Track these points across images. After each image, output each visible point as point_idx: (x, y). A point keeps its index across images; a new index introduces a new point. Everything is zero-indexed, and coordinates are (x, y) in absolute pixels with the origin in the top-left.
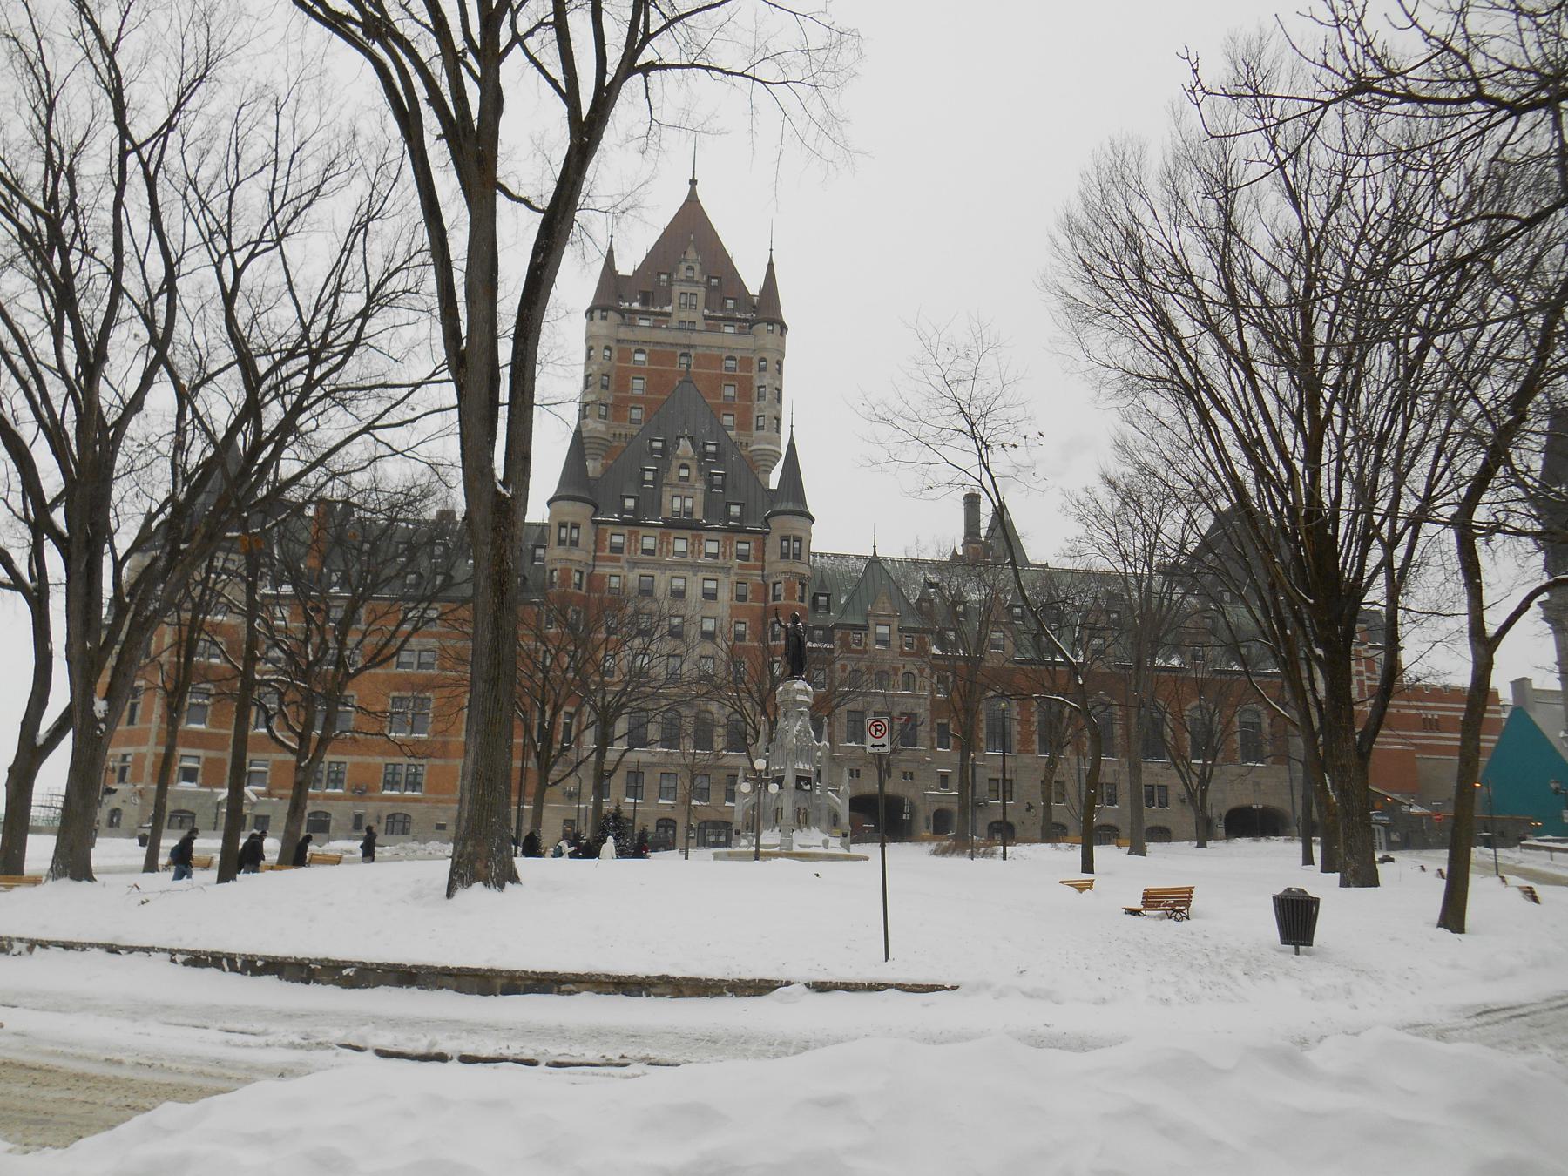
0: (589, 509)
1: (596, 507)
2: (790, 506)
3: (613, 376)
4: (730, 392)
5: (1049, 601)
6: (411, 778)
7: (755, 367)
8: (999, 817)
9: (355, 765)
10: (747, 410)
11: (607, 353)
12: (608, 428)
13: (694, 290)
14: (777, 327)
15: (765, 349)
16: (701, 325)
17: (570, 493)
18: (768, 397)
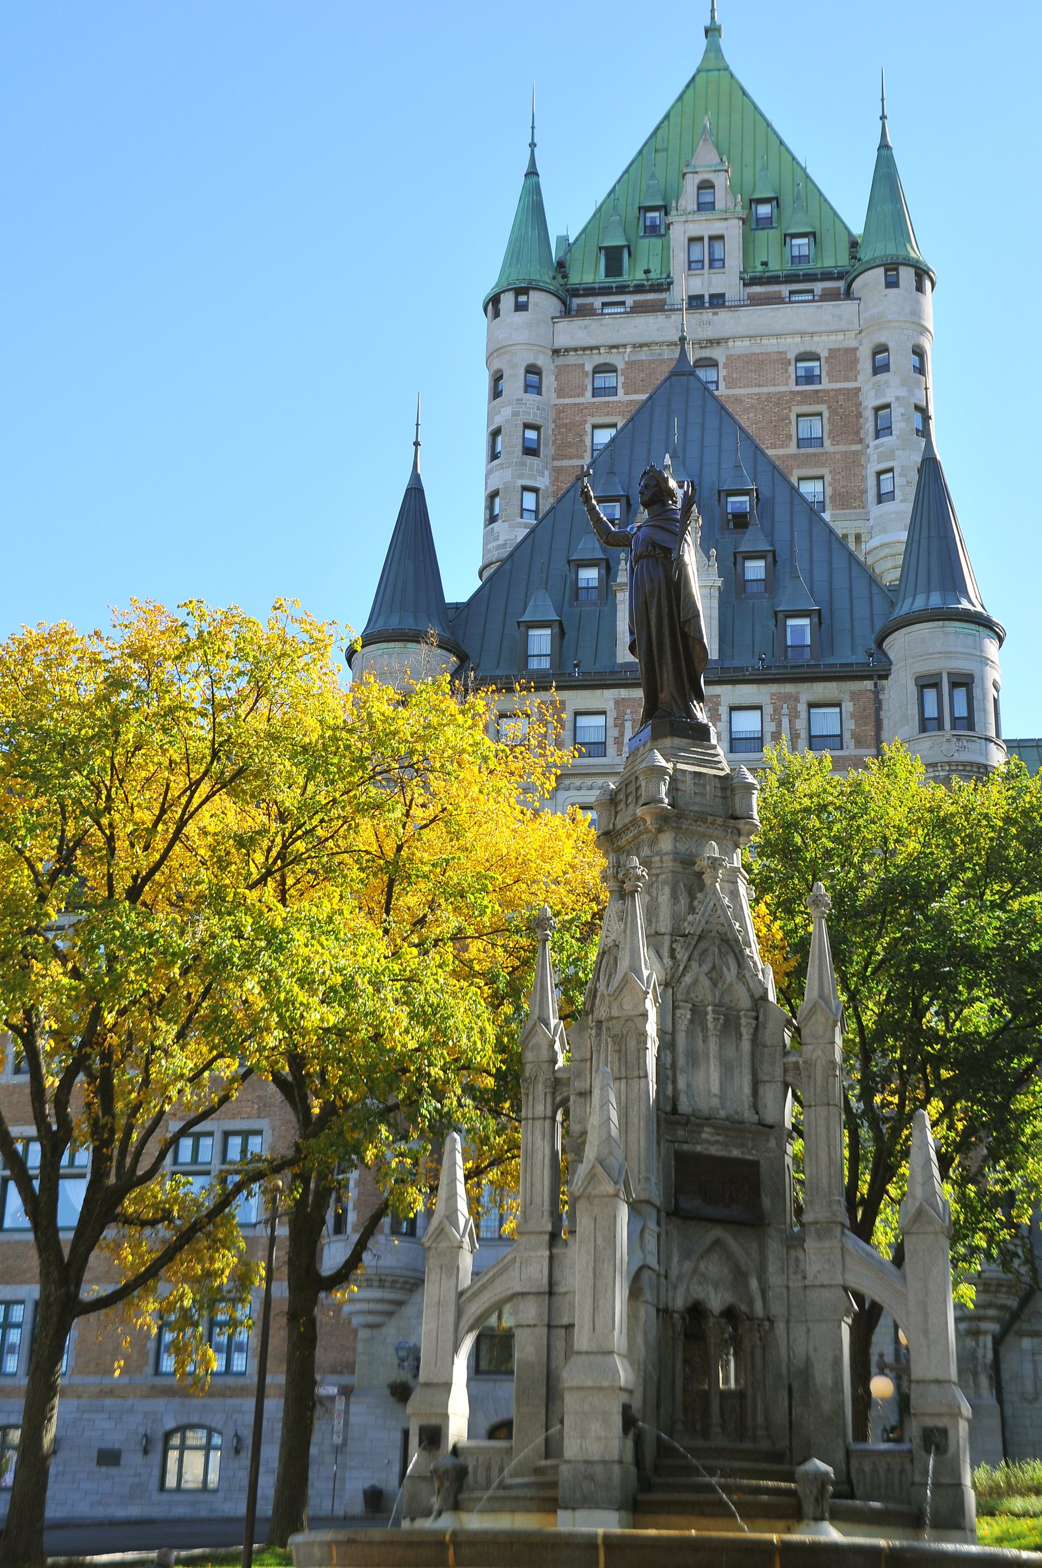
2: (936, 600)
7: (865, 365)
10: (854, 462)
13: (717, 228)
14: (907, 275)
17: (394, 623)
18: (897, 426)
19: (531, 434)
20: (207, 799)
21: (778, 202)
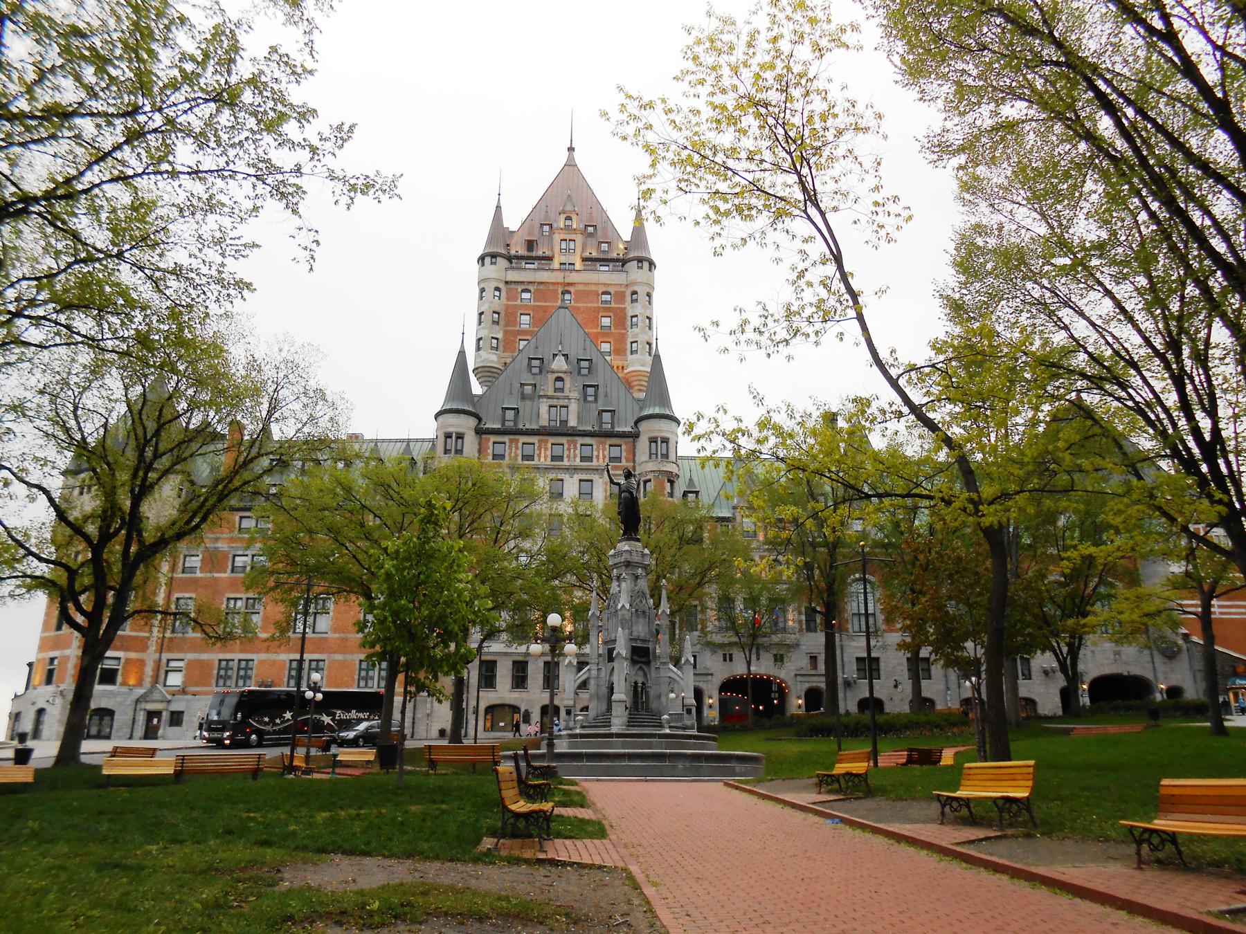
0: (472, 422)
1: (480, 419)
2: (657, 410)
3: (502, 314)
4: (606, 321)
5: (907, 462)
6: (222, 673)
7: (628, 298)
8: (867, 695)
9: (262, 662)
10: (623, 337)
11: (497, 293)
12: (500, 357)
14: (646, 265)
15: (635, 283)
16: (578, 266)
17: (454, 407)
19: (496, 316)
20: (793, 806)
21: (596, 228)
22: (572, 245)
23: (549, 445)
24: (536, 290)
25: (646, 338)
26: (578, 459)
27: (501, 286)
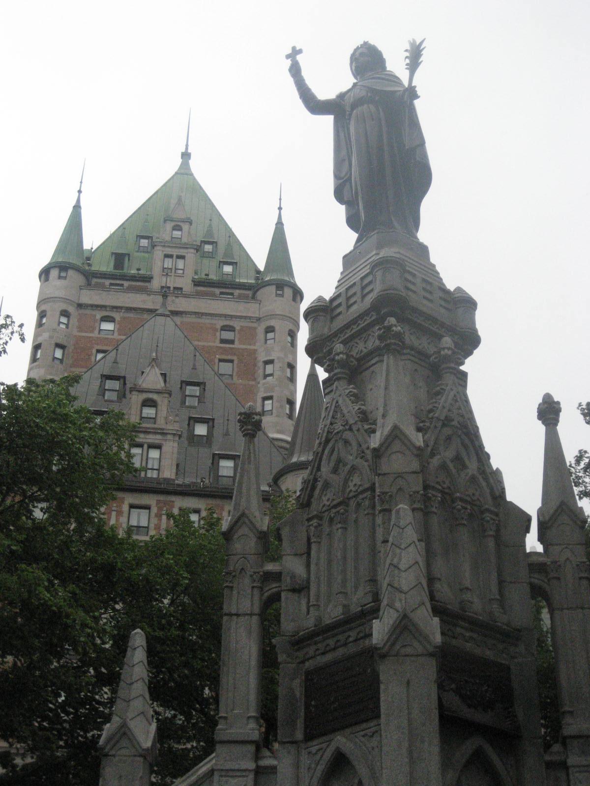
3: (71, 348)
11: (64, 320)
14: (288, 292)
21: (218, 242)
22: (180, 264)
23: (125, 508)
24: (124, 318)
25: (287, 393)
26: (218, 341)
27: (71, 309)
